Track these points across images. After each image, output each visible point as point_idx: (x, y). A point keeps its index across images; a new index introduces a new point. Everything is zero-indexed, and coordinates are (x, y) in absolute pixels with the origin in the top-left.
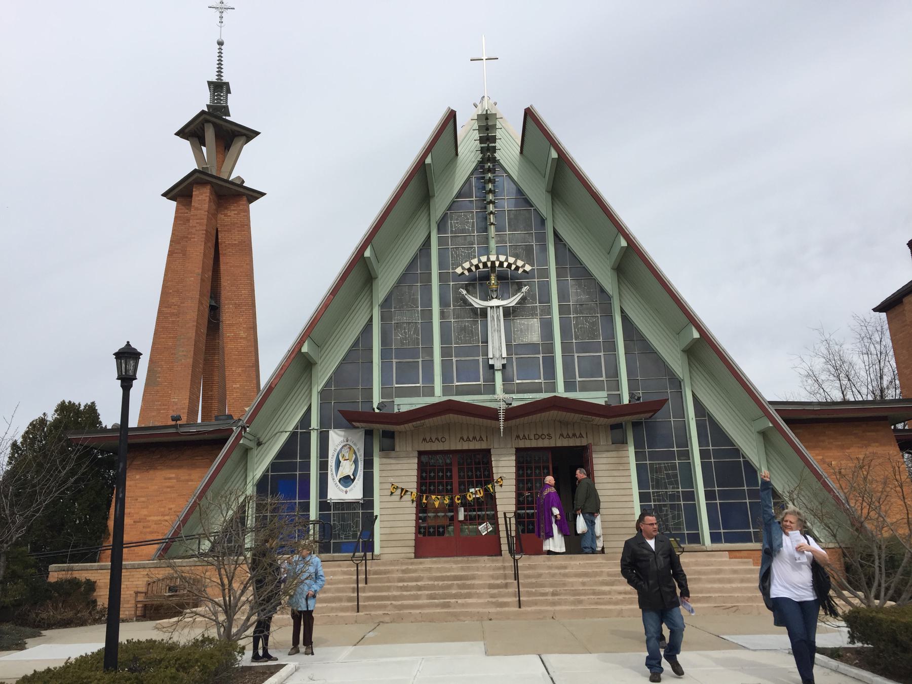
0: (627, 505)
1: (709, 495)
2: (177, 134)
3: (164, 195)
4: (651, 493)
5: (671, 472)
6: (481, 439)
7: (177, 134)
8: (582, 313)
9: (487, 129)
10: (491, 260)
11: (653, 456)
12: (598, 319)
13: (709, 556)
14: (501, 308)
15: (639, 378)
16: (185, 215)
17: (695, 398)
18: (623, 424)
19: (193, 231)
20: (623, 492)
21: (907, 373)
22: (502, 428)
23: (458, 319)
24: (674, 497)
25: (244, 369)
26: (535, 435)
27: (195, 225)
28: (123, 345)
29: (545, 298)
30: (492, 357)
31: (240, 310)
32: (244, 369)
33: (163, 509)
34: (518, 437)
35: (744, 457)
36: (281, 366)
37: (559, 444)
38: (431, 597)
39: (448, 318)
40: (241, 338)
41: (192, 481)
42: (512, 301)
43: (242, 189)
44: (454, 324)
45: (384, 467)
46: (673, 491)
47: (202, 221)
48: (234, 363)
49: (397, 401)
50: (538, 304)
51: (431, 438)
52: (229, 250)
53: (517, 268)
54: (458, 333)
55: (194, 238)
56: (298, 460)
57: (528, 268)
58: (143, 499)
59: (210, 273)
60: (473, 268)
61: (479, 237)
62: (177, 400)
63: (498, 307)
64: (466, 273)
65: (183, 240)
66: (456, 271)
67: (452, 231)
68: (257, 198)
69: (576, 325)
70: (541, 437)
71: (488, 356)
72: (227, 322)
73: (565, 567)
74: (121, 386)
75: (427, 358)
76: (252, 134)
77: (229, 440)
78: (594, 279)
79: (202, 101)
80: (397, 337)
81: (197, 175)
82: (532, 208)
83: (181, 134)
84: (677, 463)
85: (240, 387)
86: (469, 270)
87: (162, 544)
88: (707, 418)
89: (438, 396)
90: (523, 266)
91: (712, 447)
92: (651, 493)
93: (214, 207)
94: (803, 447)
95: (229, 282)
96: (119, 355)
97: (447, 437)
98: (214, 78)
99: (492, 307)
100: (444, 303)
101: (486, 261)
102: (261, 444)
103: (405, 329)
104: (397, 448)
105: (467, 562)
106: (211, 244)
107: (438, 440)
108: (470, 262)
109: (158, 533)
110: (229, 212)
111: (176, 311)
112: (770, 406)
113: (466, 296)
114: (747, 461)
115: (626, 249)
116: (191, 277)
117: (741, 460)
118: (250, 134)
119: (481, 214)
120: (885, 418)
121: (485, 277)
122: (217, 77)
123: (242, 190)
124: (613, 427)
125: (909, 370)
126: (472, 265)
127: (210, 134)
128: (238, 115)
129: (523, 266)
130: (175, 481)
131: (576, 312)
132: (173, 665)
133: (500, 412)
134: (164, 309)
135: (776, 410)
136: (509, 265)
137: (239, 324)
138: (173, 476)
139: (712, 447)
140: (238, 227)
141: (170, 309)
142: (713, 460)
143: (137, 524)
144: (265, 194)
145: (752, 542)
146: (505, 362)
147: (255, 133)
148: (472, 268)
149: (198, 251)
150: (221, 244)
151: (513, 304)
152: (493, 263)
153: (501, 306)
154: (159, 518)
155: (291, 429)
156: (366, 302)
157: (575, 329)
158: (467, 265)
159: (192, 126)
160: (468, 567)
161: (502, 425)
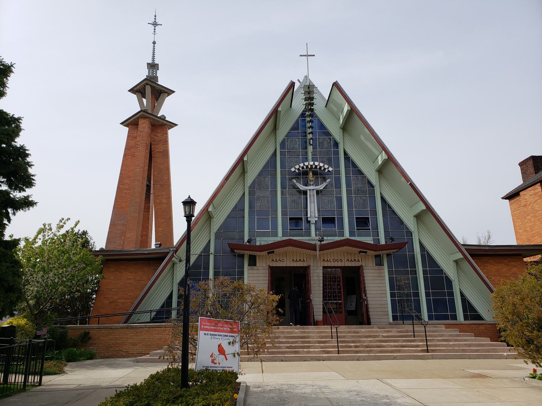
0: (382, 288)
1: (427, 294)
2: (129, 91)
3: (122, 124)
4: (396, 293)
5: (407, 281)
7: (129, 91)
8: (359, 195)
10: (301, 166)
11: (397, 272)
12: (367, 198)
14: (315, 190)
15: (390, 230)
19: (139, 143)
20: (381, 292)
22: (318, 255)
23: (291, 195)
24: (408, 295)
29: (338, 185)
30: (310, 217)
33: (126, 296)
34: (324, 260)
35: (445, 274)
36: (197, 218)
37: (347, 265)
39: (285, 195)
40: (163, 203)
41: (143, 281)
42: (321, 187)
43: (165, 122)
44: (288, 198)
46: (408, 292)
49: (258, 239)
50: (334, 189)
53: (325, 169)
56: (202, 270)
57: (330, 169)
58: (115, 290)
59: (147, 167)
60: (301, 169)
63: (313, 190)
64: (297, 171)
66: (291, 170)
67: (288, 148)
68: (173, 127)
69: (355, 201)
70: (337, 261)
73: (358, 332)
74: (186, 220)
75: (274, 216)
76: (170, 92)
78: (365, 176)
79: (143, 74)
80: (257, 205)
81: (141, 113)
82: (332, 137)
84: (410, 277)
85: (163, 230)
86: (299, 169)
88: (426, 253)
89: (280, 237)
90: (328, 168)
92: (396, 293)
93: (150, 131)
97: (285, 259)
99: (309, 190)
100: (283, 187)
102: (182, 261)
103: (262, 200)
104: (258, 265)
106: (148, 151)
109: (123, 309)
111: (127, 187)
112: (462, 246)
113: (296, 184)
114: (447, 276)
115: (386, 160)
117: (444, 275)
118: (170, 92)
119: (303, 139)
120: (520, 255)
122: (152, 61)
123: (165, 122)
124: (376, 256)
125: (522, 230)
126: (300, 166)
128: (163, 81)
129: (328, 168)
130: (133, 280)
131: (355, 193)
132: (205, 386)
133: (317, 246)
134: (121, 186)
135: (465, 249)
138: (132, 277)
141: (124, 186)
142: (429, 275)
144: (177, 125)
146: (317, 219)
147: (172, 92)
149: (142, 154)
150: (153, 152)
151: (322, 188)
152: (307, 167)
154: (124, 301)
155: (198, 253)
157: (354, 203)
158: (297, 167)
159: (138, 87)
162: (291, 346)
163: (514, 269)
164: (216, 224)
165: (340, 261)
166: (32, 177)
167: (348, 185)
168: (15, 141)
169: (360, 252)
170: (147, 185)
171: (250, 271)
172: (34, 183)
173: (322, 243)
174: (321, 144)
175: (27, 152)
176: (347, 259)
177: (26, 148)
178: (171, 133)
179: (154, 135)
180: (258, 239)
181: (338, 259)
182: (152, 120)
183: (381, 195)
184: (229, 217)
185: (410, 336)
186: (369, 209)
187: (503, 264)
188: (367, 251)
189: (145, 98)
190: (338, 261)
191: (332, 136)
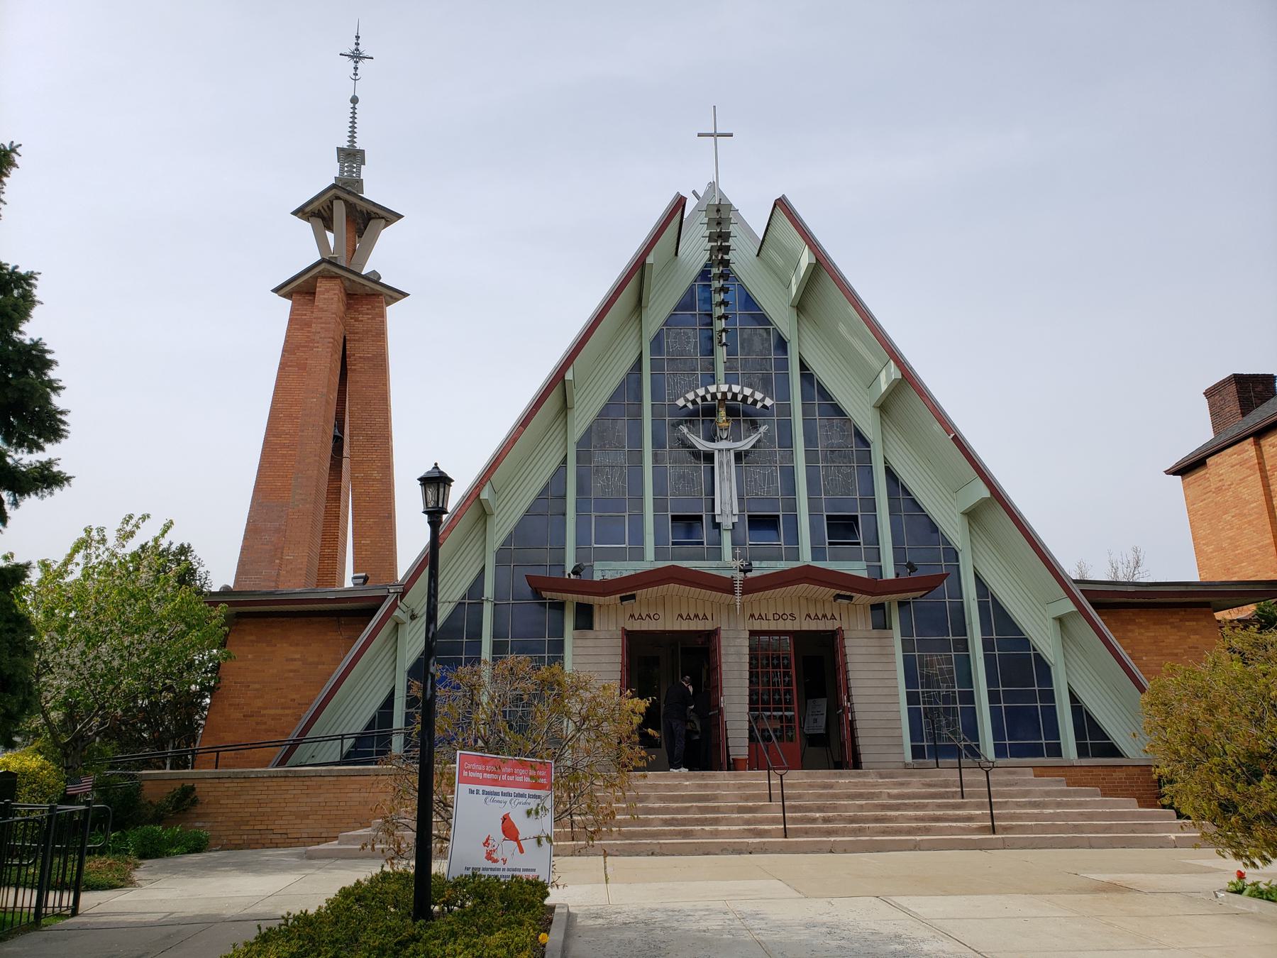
1: (993, 697)
3: (276, 290)
6: (833, 617)
7: (295, 213)
8: (834, 462)
9: (719, 224)
11: (923, 645)
13: (1010, 773)
14: (732, 452)
16: (303, 317)
17: (980, 579)
18: (886, 603)
20: (886, 691)
21: (1209, 551)
23: (676, 463)
24: (948, 698)
25: (377, 520)
26: (774, 614)
27: (320, 330)
28: (430, 468)
29: (786, 440)
31: (374, 443)
32: (377, 520)
33: (283, 700)
35: (1034, 650)
37: (805, 628)
38: (666, 822)
40: (374, 480)
42: (745, 444)
45: (578, 651)
47: (328, 325)
48: (364, 512)
49: (598, 566)
50: (777, 449)
51: (640, 615)
52: (360, 365)
53: (755, 402)
54: (675, 481)
55: (318, 347)
56: (465, 640)
57: (768, 402)
58: (257, 686)
59: (336, 395)
61: (704, 362)
62: (292, 557)
64: (690, 406)
65: (299, 349)
67: (668, 352)
68: (397, 300)
69: (826, 476)
71: (714, 512)
72: (355, 459)
73: (831, 786)
75: (636, 512)
77: (380, 611)
79: (326, 174)
80: (597, 486)
81: (323, 266)
82: (771, 327)
83: (300, 214)
86: (694, 402)
87: (284, 747)
89: (650, 562)
90: (763, 400)
91: (953, 636)
93: (343, 309)
94: (1113, 638)
95: (359, 407)
96: (426, 481)
98: (345, 144)
99: (719, 450)
100: (658, 443)
101: (726, 390)
103: (607, 475)
104: (596, 626)
105: (703, 778)
107: (650, 617)
108: (685, 397)
109: (276, 732)
110: (361, 316)
111: (288, 441)
112: (1074, 585)
113: (688, 436)
114: (1039, 654)
115: (899, 382)
116: (313, 398)
117: (1032, 652)
118: (390, 217)
119: (705, 331)
121: (710, 411)
123: (378, 288)
126: (697, 395)
127: (340, 211)
128: (375, 190)
129: (763, 400)
130: (300, 663)
131: (825, 459)
135: (1081, 590)
136: (745, 398)
137: (372, 461)
138: (298, 656)
139: (953, 636)
140: (373, 336)
142: (997, 653)
143: (248, 718)
145: (1043, 756)
148: (697, 400)
149: (324, 365)
153: (731, 449)
155: (456, 599)
156: (560, 436)
158: (691, 396)
159: (316, 204)
160: (706, 784)
161: (738, 600)
162: (673, 819)
163: (1192, 637)
164: (500, 529)
165: (790, 617)
166: (59, 416)
167: (809, 440)
168: (20, 329)
169: (838, 596)
170: (335, 436)
171: (579, 642)
172: (63, 430)
173: (749, 575)
174: (747, 343)
175: (49, 356)
176: (806, 613)
177: (46, 348)
178: (393, 313)
179: (351, 318)
180: (598, 566)
181: (784, 614)
182: (347, 283)
183: (885, 463)
184: (528, 513)
185: (953, 795)
186: (858, 496)
187: (1168, 627)
188: (853, 594)
189: (331, 230)
190: (785, 617)
191: (772, 325)
